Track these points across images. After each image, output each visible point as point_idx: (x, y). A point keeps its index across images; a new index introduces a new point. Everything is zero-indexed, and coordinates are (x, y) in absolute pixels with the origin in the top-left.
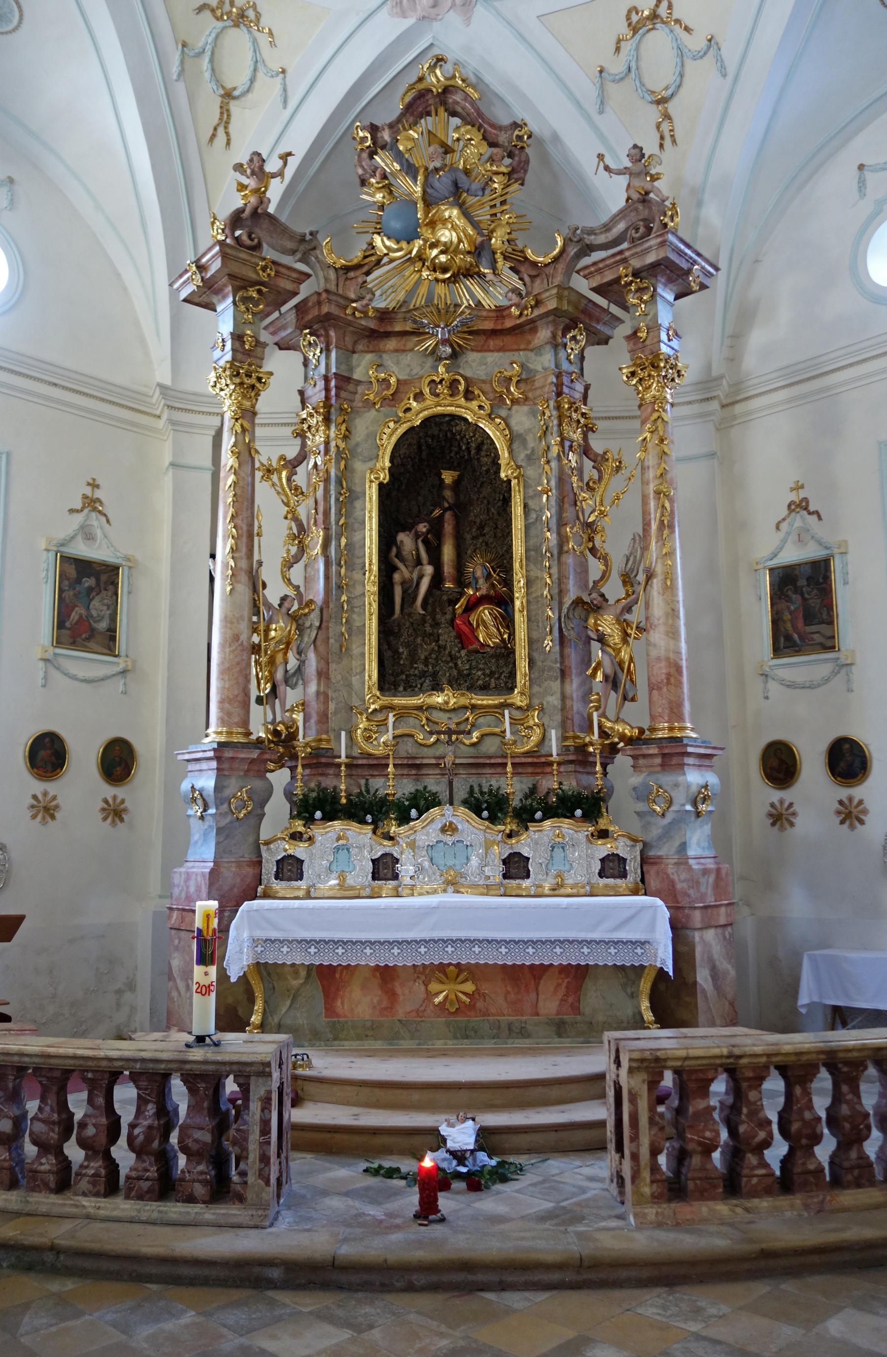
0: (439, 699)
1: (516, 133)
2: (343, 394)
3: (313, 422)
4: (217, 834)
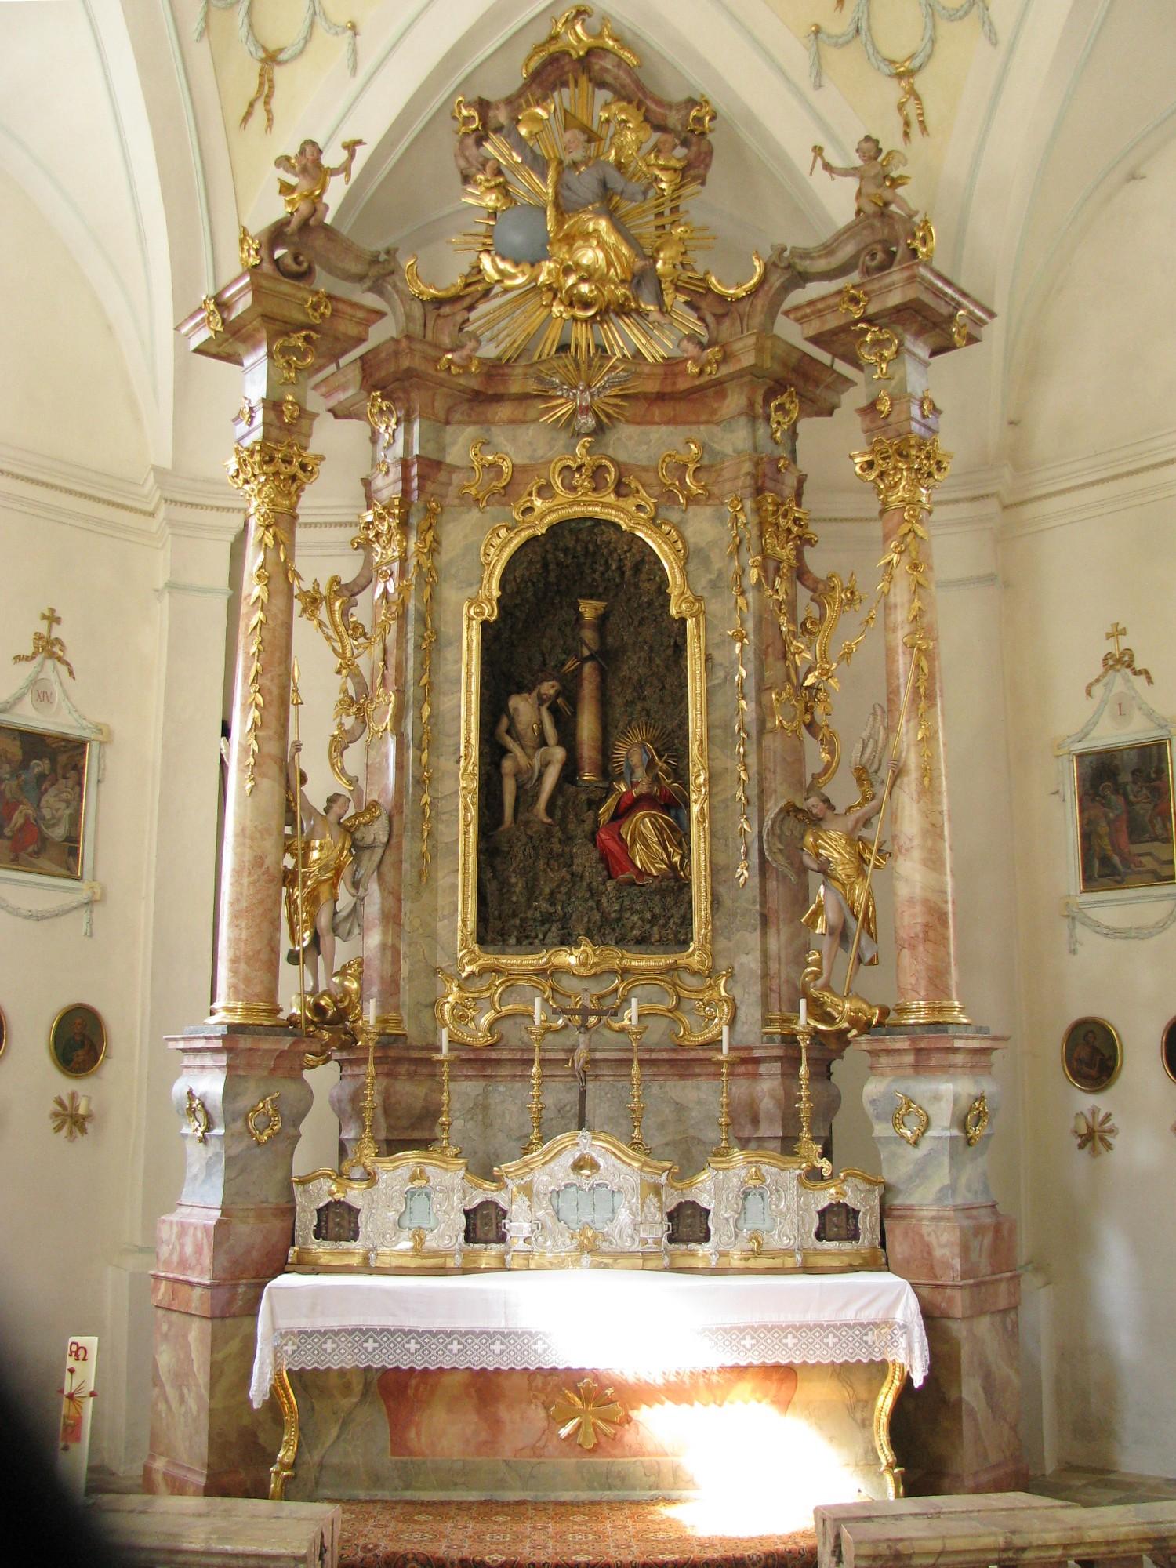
0: (570, 958)
1: (694, 113)
3: (383, 528)
4: (226, 1167)
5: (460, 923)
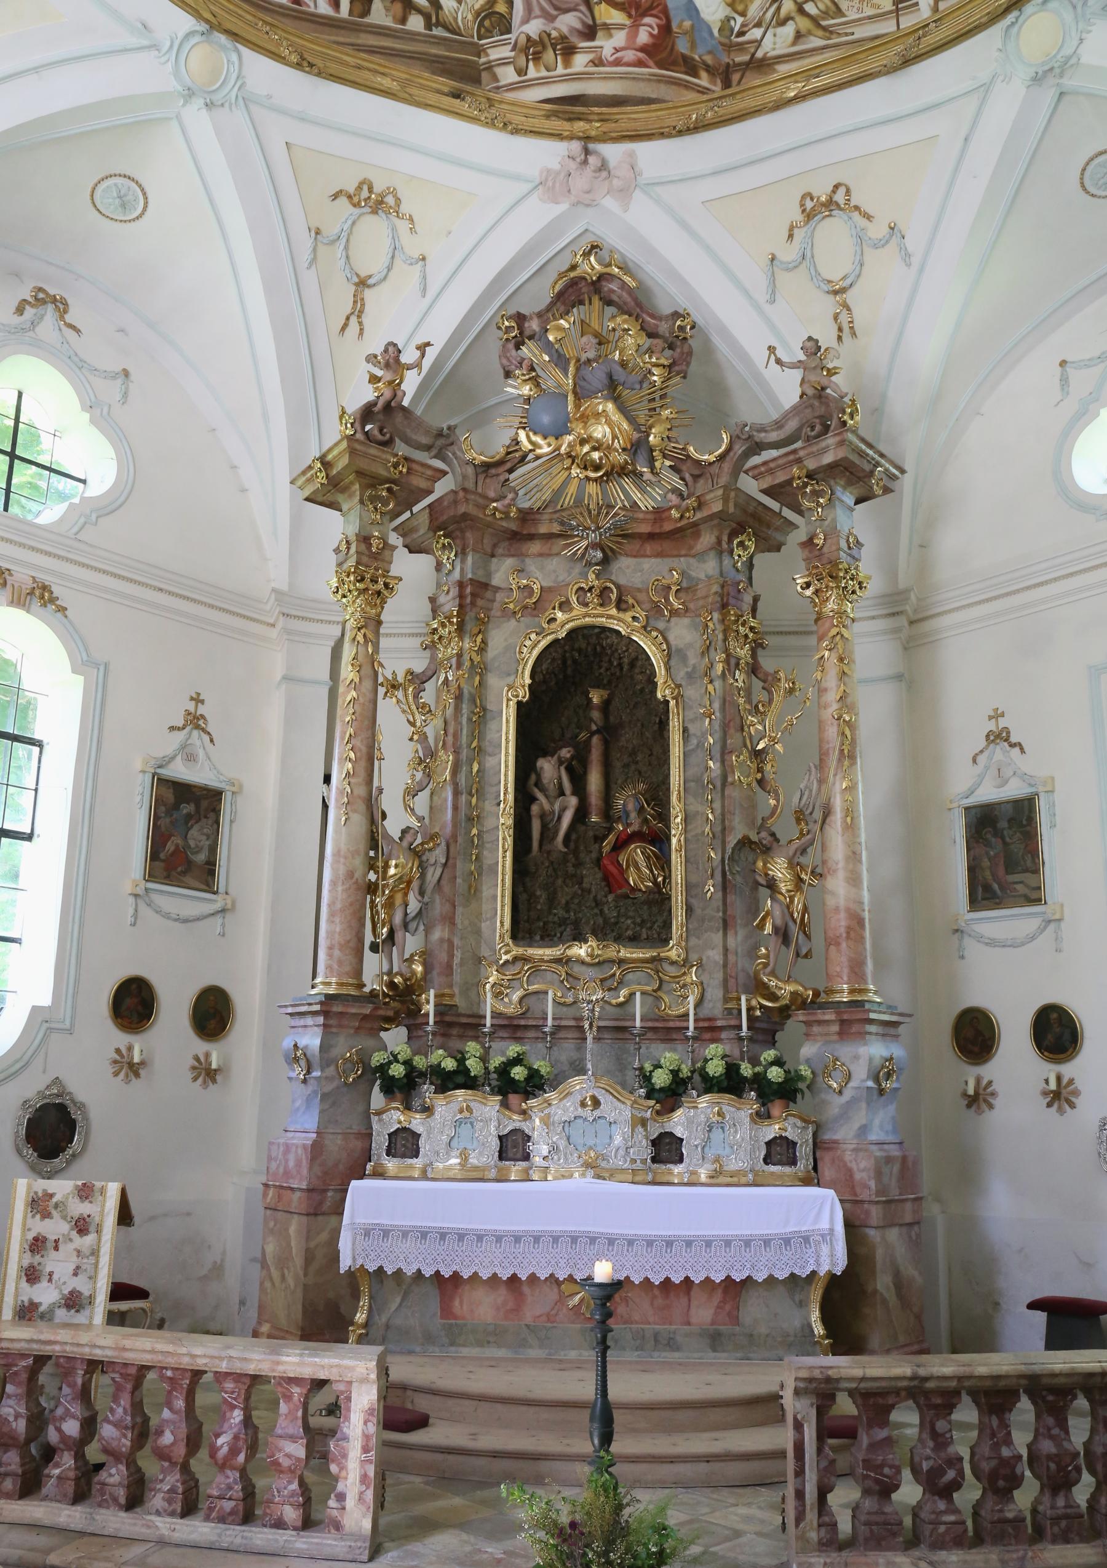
0: (580, 951)
1: (678, 323)
2: (480, 602)
3: (444, 632)
4: (321, 1100)
5: (498, 924)
